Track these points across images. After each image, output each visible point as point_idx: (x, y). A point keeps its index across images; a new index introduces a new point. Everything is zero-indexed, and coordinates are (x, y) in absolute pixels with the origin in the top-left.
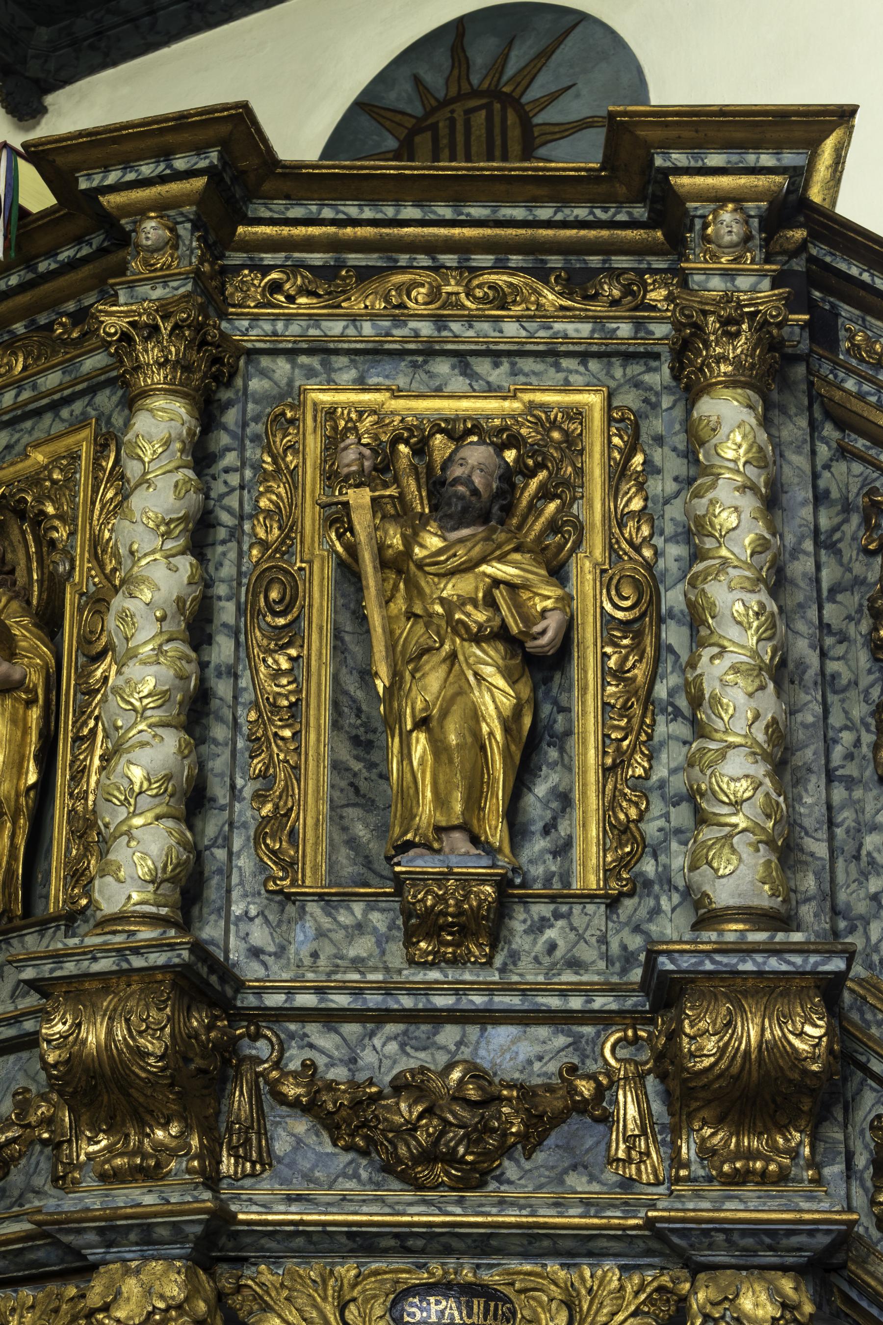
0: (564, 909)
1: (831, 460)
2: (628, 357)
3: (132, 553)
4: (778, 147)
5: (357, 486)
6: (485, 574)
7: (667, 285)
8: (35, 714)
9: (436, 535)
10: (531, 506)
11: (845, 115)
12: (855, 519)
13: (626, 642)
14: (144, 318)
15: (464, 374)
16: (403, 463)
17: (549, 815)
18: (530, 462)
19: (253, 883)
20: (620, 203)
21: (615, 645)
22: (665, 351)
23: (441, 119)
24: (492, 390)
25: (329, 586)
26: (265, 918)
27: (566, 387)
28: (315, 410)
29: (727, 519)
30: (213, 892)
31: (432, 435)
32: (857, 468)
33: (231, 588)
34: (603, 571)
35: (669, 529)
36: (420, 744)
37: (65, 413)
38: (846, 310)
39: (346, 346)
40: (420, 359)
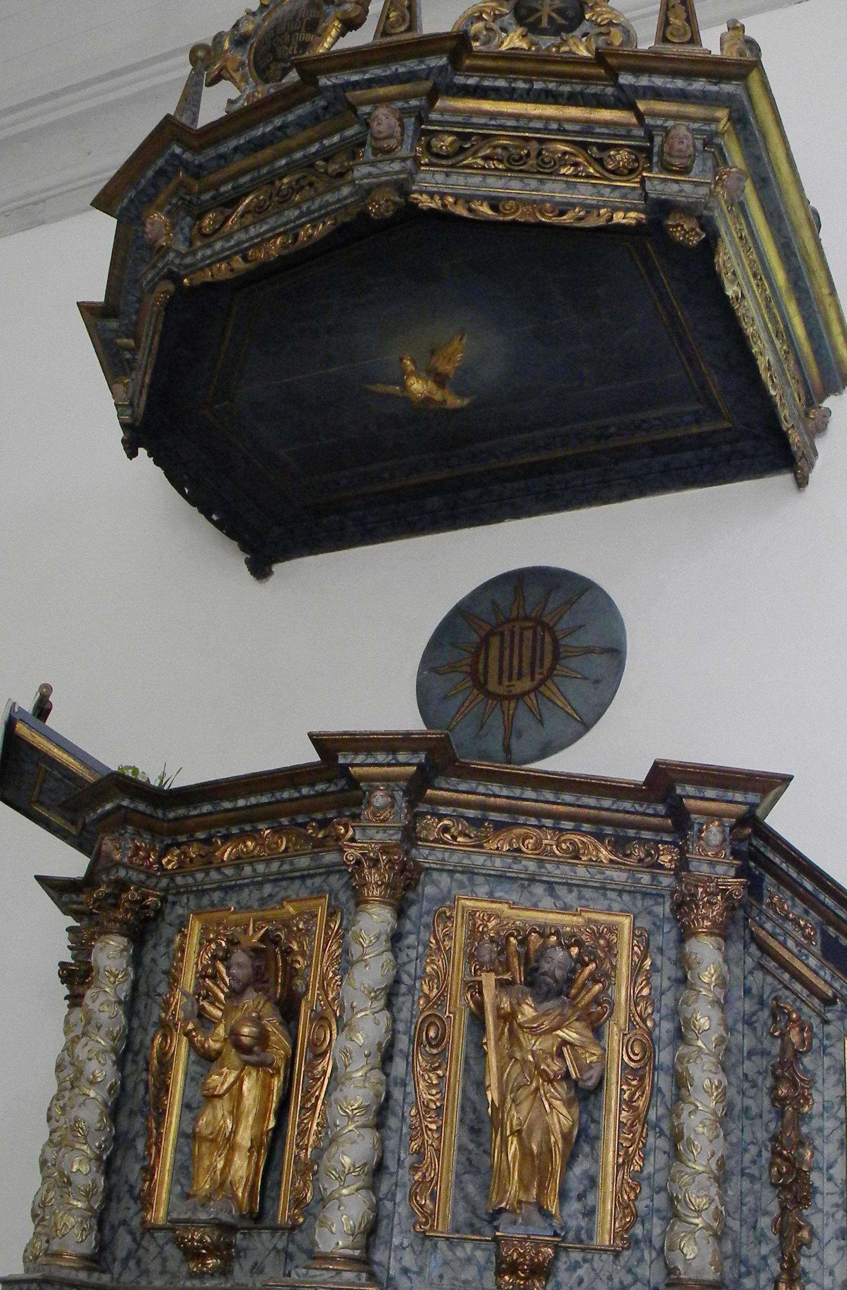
0: (589, 1256)
1: (754, 969)
2: (645, 895)
3: (352, 1008)
4: (746, 790)
5: (487, 972)
6: (558, 1035)
7: (671, 853)
8: (277, 1083)
9: (530, 1006)
10: (584, 985)
11: (786, 780)
12: (766, 1013)
13: (635, 1083)
14: (372, 854)
15: (551, 895)
16: (512, 949)
17: (582, 1188)
18: (586, 959)
19: (407, 1225)
20: (650, 802)
21: (629, 1085)
22: (667, 893)
23: (506, 628)
24: (566, 909)
25: (464, 1030)
26: (413, 1248)
27: (609, 911)
28: (463, 911)
29: (703, 1022)
30: (383, 1231)
31: (530, 933)
32: (769, 979)
33: (406, 1024)
34: (624, 1035)
35: (664, 1011)
36: (513, 1146)
37: (309, 882)
38: (768, 879)
39: (484, 872)
40: (526, 883)
